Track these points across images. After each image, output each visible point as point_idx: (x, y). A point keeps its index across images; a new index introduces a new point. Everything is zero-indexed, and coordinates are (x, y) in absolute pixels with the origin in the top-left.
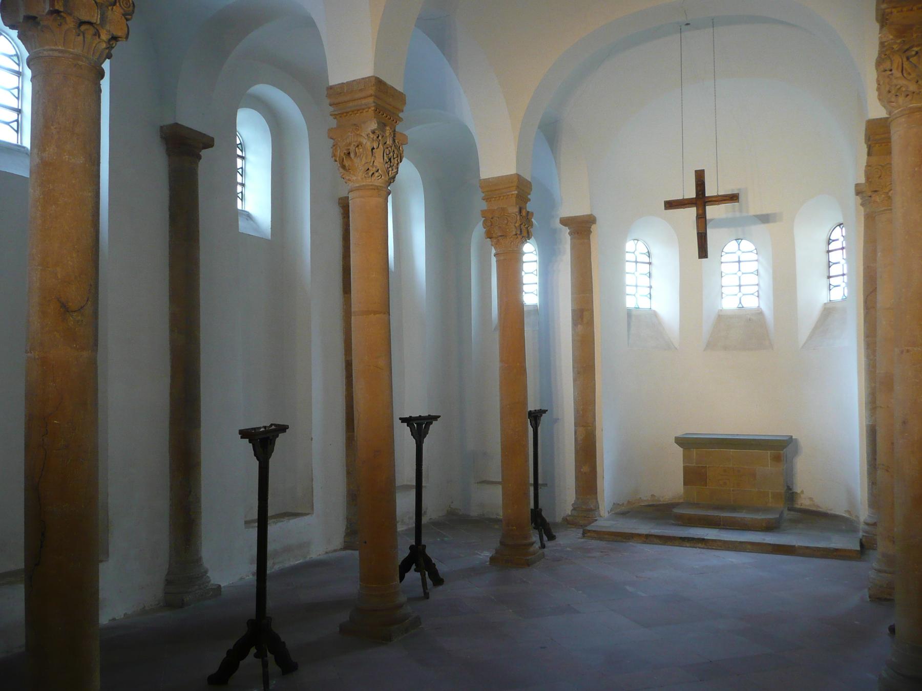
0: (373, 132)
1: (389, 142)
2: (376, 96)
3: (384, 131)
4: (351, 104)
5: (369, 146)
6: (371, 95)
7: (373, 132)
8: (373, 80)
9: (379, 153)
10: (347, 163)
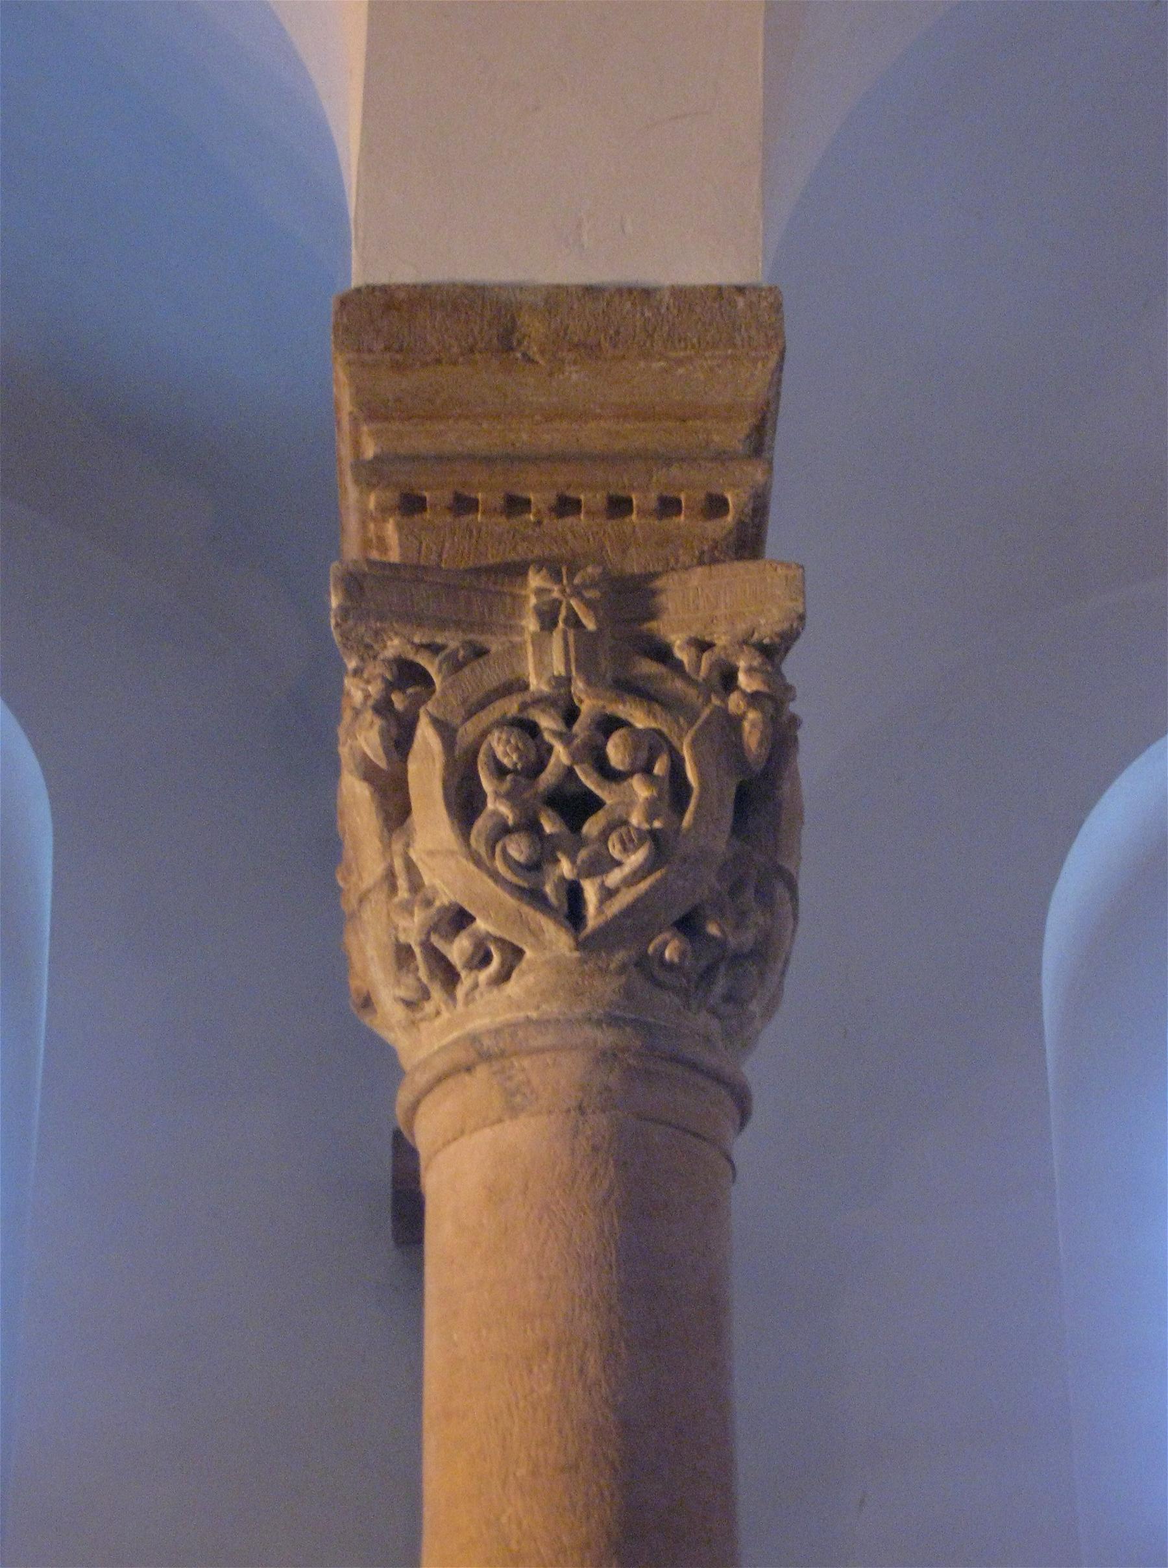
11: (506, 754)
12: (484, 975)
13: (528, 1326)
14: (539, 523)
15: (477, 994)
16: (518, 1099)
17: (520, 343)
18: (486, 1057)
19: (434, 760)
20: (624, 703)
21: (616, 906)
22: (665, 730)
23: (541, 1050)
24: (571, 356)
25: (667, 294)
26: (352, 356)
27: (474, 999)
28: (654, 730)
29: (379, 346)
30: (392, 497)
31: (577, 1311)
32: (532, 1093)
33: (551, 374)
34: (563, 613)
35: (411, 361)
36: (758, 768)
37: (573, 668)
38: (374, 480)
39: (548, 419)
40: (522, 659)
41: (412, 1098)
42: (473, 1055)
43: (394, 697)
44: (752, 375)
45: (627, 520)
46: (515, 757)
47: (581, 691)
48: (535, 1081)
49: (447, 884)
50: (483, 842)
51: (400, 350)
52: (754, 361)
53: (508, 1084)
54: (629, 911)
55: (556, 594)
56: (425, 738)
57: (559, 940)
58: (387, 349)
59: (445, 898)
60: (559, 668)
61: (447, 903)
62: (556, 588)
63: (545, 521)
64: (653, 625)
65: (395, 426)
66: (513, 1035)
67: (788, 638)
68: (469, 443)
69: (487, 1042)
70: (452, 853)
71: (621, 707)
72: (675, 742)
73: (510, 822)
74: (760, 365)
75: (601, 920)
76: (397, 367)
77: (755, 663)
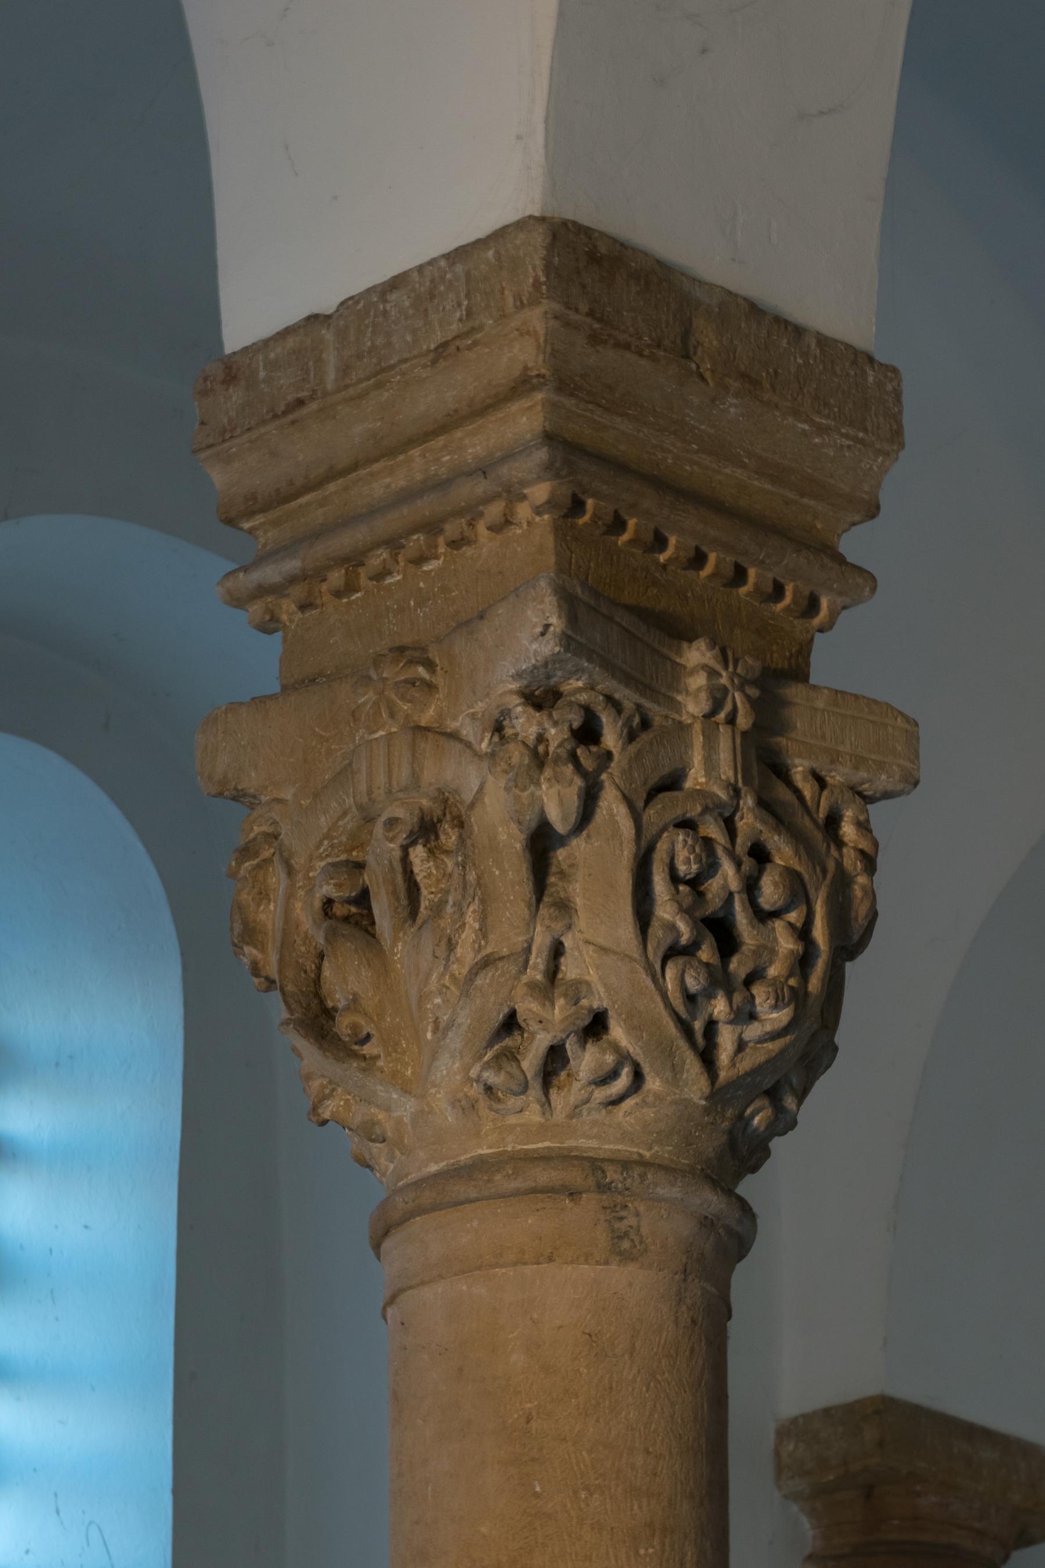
0: (541, 698)
1: (709, 768)
2: (565, 385)
3: (657, 681)
4: (383, 482)
5: (498, 819)
6: (522, 386)
7: (541, 698)
8: (539, 238)
9: (597, 864)
10: (346, 980)
11: (688, 862)
12: (601, 1094)
13: (636, 1503)
14: (664, 567)
16: (626, 1245)
19: (621, 844)
20: (779, 835)
21: (746, 1064)
22: (806, 877)
26: (556, 307)
27: (580, 1114)
28: (796, 871)
29: (584, 308)
31: (679, 1497)
32: (641, 1242)
33: (713, 400)
37: (740, 777)
38: (564, 473)
43: (579, 751)
45: (734, 591)
46: (695, 867)
47: (748, 808)
48: (645, 1230)
51: (600, 320)
53: (617, 1225)
55: (724, 680)
57: (695, 1086)
58: (588, 314)
59: (598, 1000)
60: (727, 771)
61: (595, 1007)
64: (779, 739)
65: (570, 403)
68: (622, 447)
70: (632, 959)
71: (776, 838)
75: (733, 1073)
76: (594, 339)
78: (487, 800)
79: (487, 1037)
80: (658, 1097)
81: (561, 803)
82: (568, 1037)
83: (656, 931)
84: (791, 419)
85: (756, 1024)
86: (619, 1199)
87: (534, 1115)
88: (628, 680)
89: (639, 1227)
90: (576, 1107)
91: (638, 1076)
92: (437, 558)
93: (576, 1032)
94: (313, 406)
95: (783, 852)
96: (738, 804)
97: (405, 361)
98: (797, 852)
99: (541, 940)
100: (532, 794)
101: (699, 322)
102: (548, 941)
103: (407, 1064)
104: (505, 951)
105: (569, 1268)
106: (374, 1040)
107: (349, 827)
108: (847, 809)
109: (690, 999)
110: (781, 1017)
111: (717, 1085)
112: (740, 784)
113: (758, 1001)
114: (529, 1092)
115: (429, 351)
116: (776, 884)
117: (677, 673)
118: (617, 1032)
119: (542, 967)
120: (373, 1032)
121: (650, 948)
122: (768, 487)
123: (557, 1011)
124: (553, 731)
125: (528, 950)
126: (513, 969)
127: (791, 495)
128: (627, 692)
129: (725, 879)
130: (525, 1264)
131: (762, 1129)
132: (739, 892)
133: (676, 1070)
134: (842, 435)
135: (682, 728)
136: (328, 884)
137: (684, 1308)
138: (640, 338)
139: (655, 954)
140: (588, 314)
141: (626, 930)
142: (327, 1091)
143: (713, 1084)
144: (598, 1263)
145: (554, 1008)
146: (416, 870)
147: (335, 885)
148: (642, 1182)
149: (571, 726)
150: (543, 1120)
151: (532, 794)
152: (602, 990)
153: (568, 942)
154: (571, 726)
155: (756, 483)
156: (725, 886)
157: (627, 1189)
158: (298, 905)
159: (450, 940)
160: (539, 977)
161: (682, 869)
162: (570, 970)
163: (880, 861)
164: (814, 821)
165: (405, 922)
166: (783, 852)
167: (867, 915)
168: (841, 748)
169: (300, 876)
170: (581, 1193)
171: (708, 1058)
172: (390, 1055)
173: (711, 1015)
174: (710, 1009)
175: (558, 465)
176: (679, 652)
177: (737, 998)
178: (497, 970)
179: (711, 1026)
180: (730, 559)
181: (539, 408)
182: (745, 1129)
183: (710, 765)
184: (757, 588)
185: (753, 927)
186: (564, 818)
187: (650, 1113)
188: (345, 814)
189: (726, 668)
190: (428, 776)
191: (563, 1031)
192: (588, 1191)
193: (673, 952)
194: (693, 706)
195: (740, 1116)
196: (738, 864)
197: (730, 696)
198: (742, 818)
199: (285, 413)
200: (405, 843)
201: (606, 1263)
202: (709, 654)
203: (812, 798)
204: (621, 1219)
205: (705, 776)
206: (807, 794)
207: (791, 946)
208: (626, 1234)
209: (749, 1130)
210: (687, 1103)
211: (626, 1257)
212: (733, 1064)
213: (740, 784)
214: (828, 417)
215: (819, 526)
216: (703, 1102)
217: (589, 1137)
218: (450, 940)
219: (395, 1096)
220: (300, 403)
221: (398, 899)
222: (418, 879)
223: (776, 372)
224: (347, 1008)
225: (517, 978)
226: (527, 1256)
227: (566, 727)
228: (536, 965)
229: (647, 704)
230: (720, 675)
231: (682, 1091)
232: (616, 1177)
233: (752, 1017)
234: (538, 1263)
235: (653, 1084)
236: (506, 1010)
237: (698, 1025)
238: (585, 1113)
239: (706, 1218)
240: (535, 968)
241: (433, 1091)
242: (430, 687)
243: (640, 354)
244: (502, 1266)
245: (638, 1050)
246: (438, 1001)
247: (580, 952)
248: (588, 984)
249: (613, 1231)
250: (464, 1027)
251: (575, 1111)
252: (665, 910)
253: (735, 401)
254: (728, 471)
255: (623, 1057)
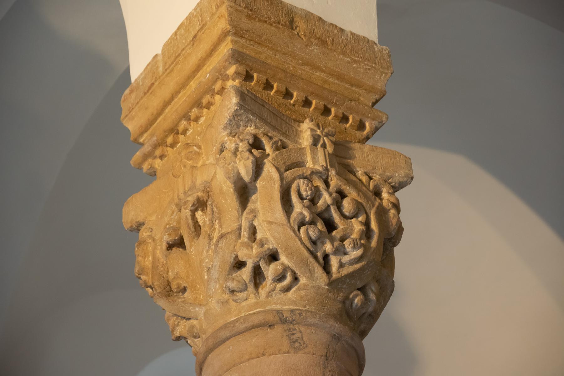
1: (314, 161)
11: (306, 190)
12: (279, 286)
14: (294, 105)
15: (274, 293)
16: (297, 345)
17: (296, 28)
18: (283, 321)
20: (349, 187)
22: (364, 204)
23: (311, 325)
24: (316, 41)
25: (349, 34)
26: (232, 4)
27: (272, 296)
28: (360, 202)
30: (242, 69)
32: (304, 343)
33: (307, 46)
34: (321, 142)
35: (254, 17)
36: (393, 234)
37: (328, 165)
39: (304, 64)
40: (305, 154)
41: (224, 337)
42: (277, 319)
44: (380, 78)
45: (327, 118)
46: (309, 192)
48: (305, 339)
49: (275, 238)
50: (296, 223)
51: (251, 10)
52: (382, 73)
54: (350, 276)
55: (318, 132)
56: (269, 172)
58: (245, 8)
59: (272, 244)
61: (271, 248)
62: (318, 131)
63: (296, 106)
65: (243, 41)
66: (300, 314)
67: (170, 247)
69: (286, 315)
70: (283, 225)
71: (348, 188)
72: (368, 211)
73: (307, 219)
74: (384, 75)
75: (339, 275)
76: (249, 17)
77: (390, 191)
78: (217, 176)
79: (228, 269)
80: (305, 285)
81: (245, 166)
82: (260, 260)
83: (294, 215)
84: (342, 56)
85: (347, 256)
86: (292, 326)
87: (252, 300)
88: (274, 128)
89: (302, 337)
90: (270, 292)
91: (296, 279)
92: (203, 116)
93: (264, 259)
94: (157, 83)
95: (352, 193)
96: (328, 174)
97: (183, 49)
98: (359, 194)
99: (245, 225)
100: (233, 166)
101: (297, 19)
102: (248, 224)
103: (201, 294)
104: (230, 230)
105: (272, 357)
106: (188, 291)
107: (176, 218)
108: (383, 187)
109: (314, 243)
110: (358, 252)
111: (332, 279)
112: (329, 167)
113: (346, 246)
114: (248, 289)
115: (190, 41)
116: (349, 203)
117: (297, 134)
118: (283, 259)
119: (247, 236)
120: (186, 285)
121: (291, 221)
122: (336, 81)
123: (254, 251)
124: (241, 144)
125: (240, 229)
126: (234, 237)
127: (347, 86)
128: (274, 133)
129: (325, 199)
130: (253, 358)
131: (359, 304)
132: (332, 205)
133: (312, 272)
134: (365, 64)
135: (302, 150)
136: (165, 235)
137: (327, 370)
138: (270, 19)
139: (294, 223)
140: (245, 8)
141: (279, 213)
142: (176, 323)
143: (329, 279)
144: (284, 353)
145: (252, 250)
146: (199, 220)
147: (168, 235)
148: (300, 317)
149: (248, 142)
150: (255, 300)
151: (233, 166)
152: (272, 239)
153: (256, 223)
154: (248, 142)
155: (331, 79)
156: (325, 202)
157: (294, 320)
158: (158, 252)
159: (209, 236)
160: (246, 240)
161: (304, 194)
162: (259, 236)
163: (401, 206)
164: (369, 190)
165: (194, 238)
166: (352, 193)
167: (396, 224)
168: (377, 165)
169: (158, 241)
170: (274, 325)
171: (326, 267)
172: (193, 292)
173: (325, 251)
174: (324, 248)
175: (236, 56)
176: (299, 126)
177: (336, 244)
178: (227, 239)
179: (326, 257)
180: (322, 103)
181: (230, 43)
182: (351, 305)
183: (315, 161)
184: (336, 116)
185: (341, 220)
186: (247, 173)
187: (303, 293)
188: (173, 212)
189: (319, 128)
190: (199, 181)
191: (257, 257)
192: (277, 323)
193: (302, 224)
194: (306, 140)
195: (347, 298)
196: (330, 194)
197: (322, 139)
198: (331, 180)
199: (148, 91)
200: (192, 208)
201: (288, 352)
202: (310, 124)
203: (366, 182)
204: (293, 334)
205: (313, 164)
206: (364, 181)
207: (360, 227)
208: (297, 341)
209: (354, 305)
210: (319, 287)
211: (296, 350)
212: (338, 272)
213: (329, 167)
214: (358, 57)
215: (362, 99)
216: (327, 287)
217: (277, 304)
218: (209, 236)
219: (197, 309)
220: (153, 84)
221: (190, 229)
222: (200, 224)
223: (333, 39)
224: (174, 278)
225: (236, 241)
226: (253, 355)
227: (246, 142)
228: (244, 235)
229: (285, 140)
230: (316, 131)
231: (316, 282)
232: (288, 315)
233: (345, 253)
234: (258, 357)
235: (303, 280)
236: (234, 256)
237: (319, 254)
238: (274, 295)
239: (335, 335)
240: (244, 236)
241: (210, 300)
242: (199, 154)
243: (271, 25)
244: (243, 362)
245: (293, 264)
246: (207, 260)
247: (262, 226)
248: (267, 238)
249: (290, 340)
250: (218, 267)
251: (269, 294)
252: (298, 207)
253: (316, 47)
254: (318, 74)
255: (286, 269)
